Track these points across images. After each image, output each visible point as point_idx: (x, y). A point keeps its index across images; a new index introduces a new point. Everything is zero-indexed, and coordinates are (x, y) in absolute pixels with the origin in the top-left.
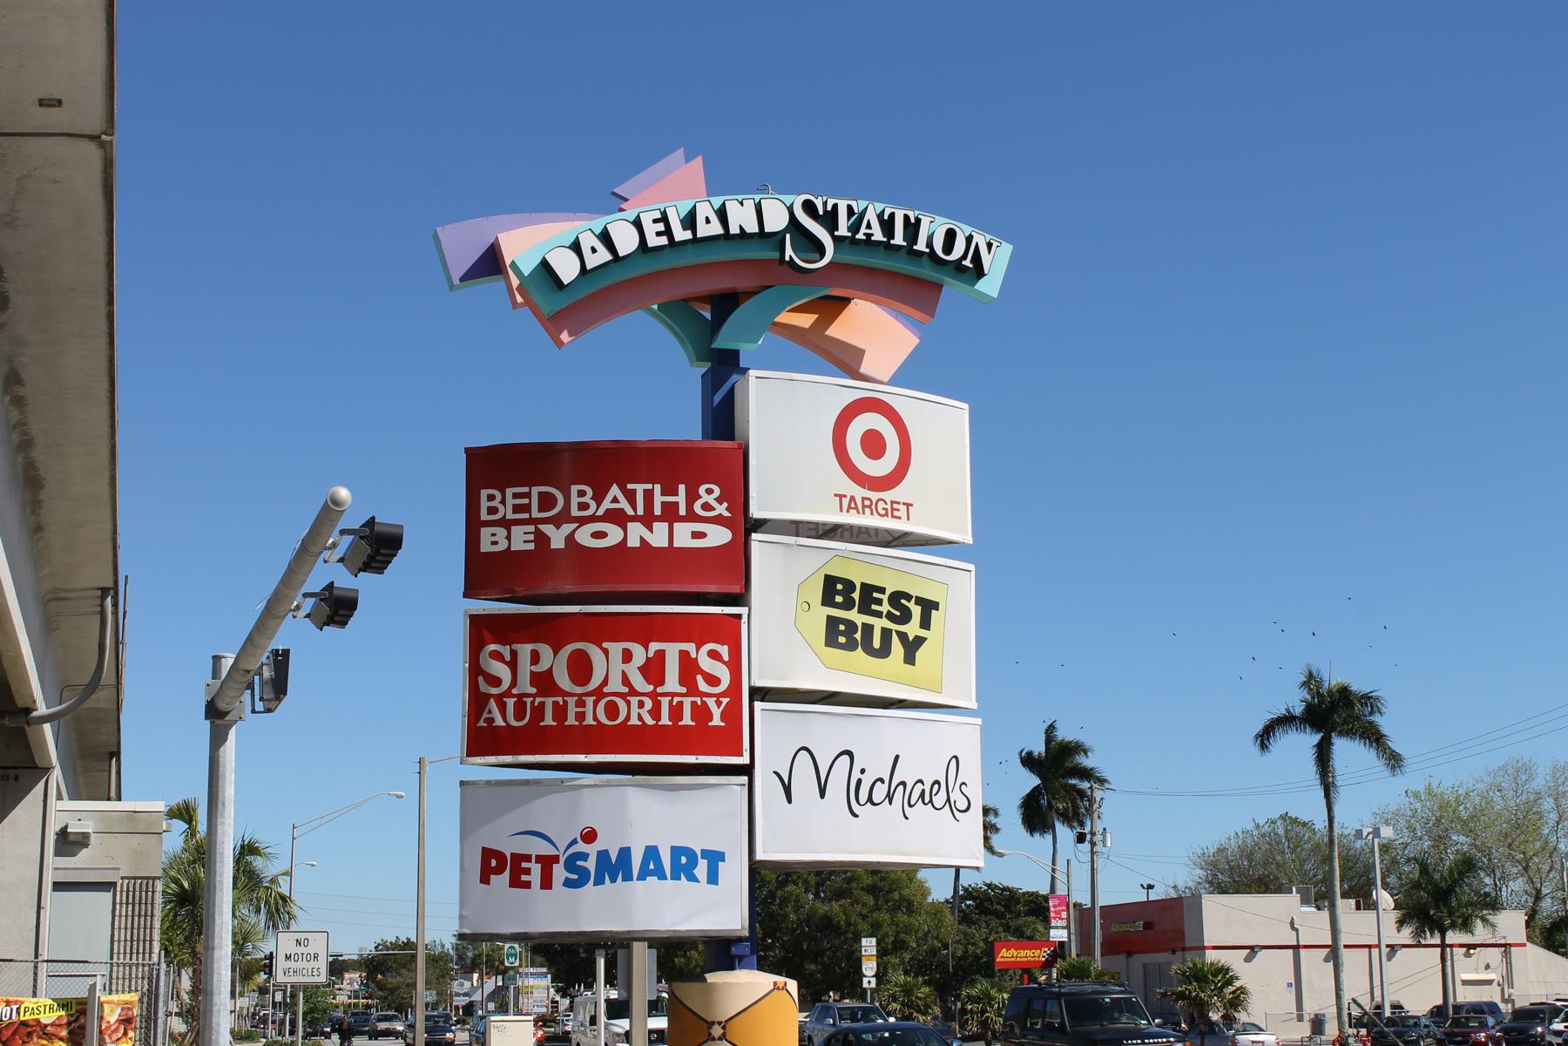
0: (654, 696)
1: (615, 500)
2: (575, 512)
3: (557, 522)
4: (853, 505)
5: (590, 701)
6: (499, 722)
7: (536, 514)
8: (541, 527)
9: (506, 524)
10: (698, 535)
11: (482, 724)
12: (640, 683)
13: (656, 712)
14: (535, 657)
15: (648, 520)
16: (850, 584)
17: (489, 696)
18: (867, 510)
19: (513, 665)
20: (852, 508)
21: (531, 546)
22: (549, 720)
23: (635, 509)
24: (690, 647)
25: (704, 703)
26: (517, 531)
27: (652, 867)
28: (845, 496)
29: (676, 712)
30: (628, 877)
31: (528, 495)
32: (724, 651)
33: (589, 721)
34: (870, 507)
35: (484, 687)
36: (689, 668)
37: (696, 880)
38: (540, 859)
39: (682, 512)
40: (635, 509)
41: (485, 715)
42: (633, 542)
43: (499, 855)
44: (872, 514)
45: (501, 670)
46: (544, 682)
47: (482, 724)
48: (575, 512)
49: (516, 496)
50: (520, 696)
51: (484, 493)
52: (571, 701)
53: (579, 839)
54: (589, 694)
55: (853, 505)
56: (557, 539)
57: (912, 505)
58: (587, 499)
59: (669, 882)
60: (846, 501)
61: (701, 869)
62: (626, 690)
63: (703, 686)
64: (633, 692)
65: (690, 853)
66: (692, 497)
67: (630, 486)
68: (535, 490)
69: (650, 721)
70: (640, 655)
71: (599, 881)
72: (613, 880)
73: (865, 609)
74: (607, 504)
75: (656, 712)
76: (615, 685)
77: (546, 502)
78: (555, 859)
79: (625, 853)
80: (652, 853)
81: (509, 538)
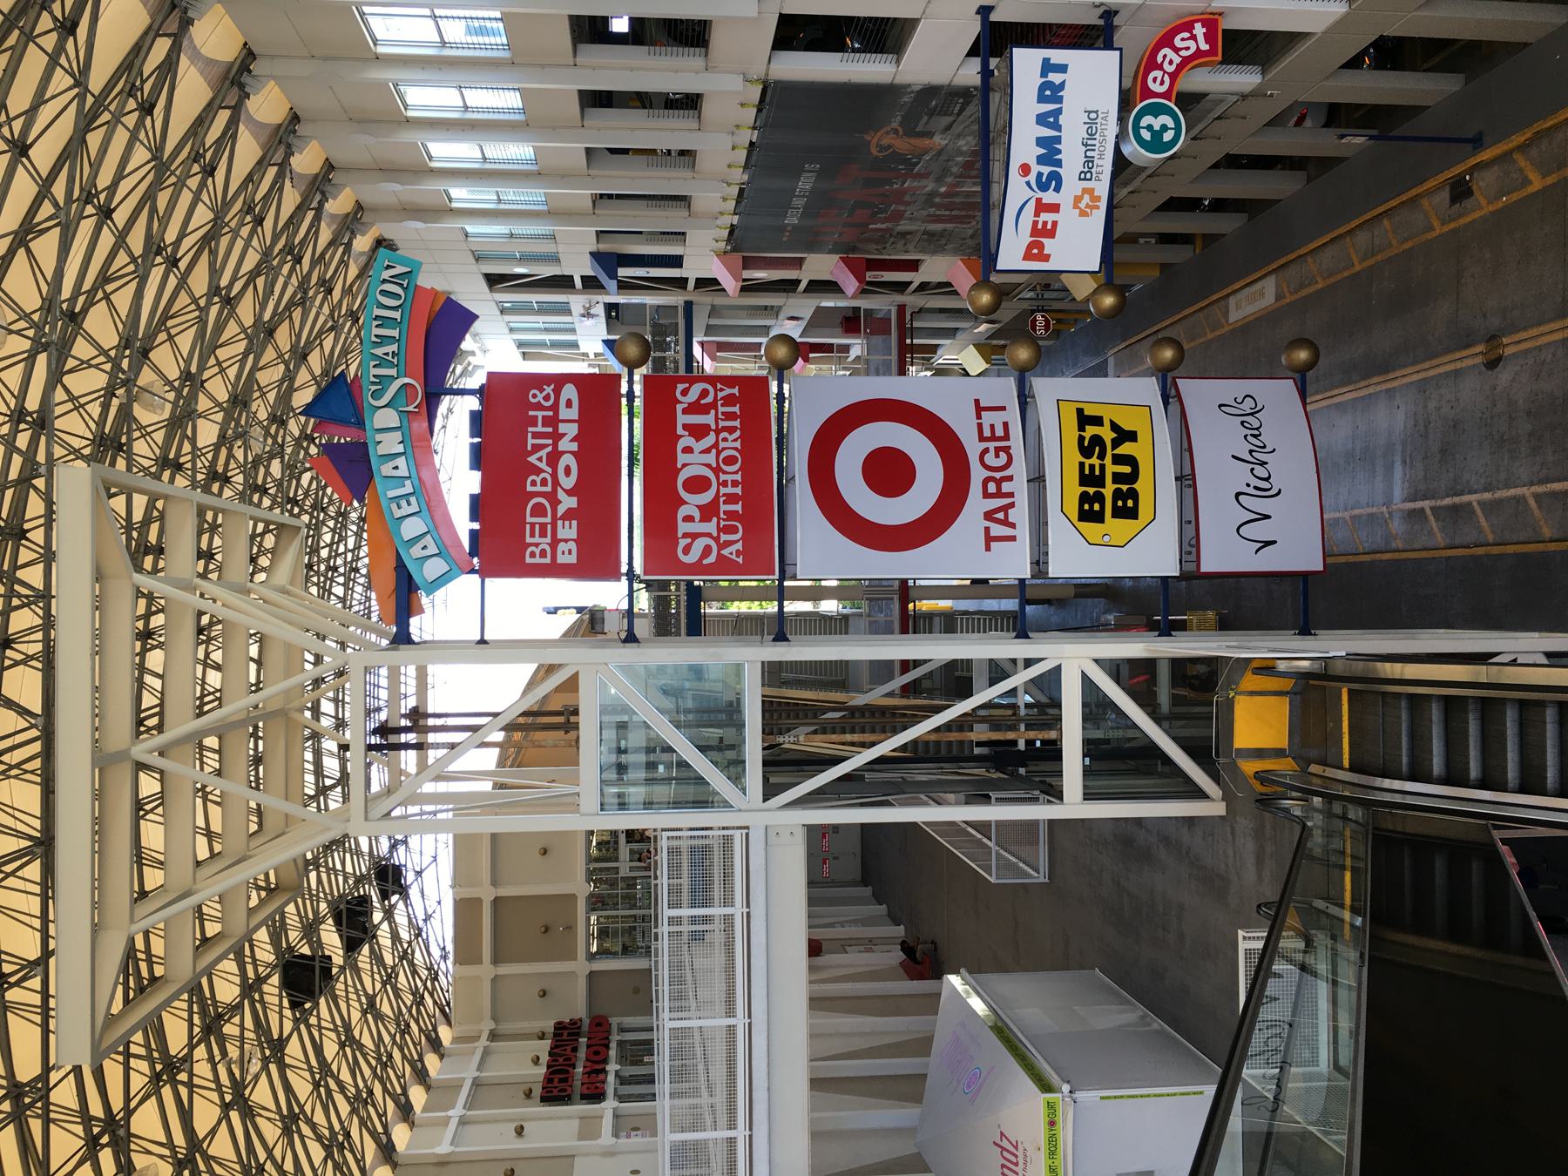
0: (718, 432)
1: (540, 459)
2: (549, 489)
3: (555, 502)
4: (1001, 516)
5: (723, 477)
6: (739, 546)
7: (548, 519)
8: (559, 515)
9: (555, 543)
10: (569, 404)
11: (740, 560)
12: (710, 440)
13: (731, 430)
14: (688, 519)
15: (557, 437)
16: (1084, 498)
18: (1006, 487)
19: (694, 536)
20: (1006, 516)
21: (574, 523)
22: (738, 507)
23: (547, 446)
24: (679, 408)
25: (721, 399)
27: (1052, 120)
28: (987, 530)
29: (729, 416)
30: (1058, 140)
32: (680, 387)
33: (738, 477)
35: (712, 559)
36: (693, 408)
37: (1063, 83)
38: (1037, 214)
39: (551, 413)
40: (547, 446)
41: (734, 557)
42: (574, 447)
43: (1030, 246)
44: (1010, 478)
45: (699, 545)
46: (708, 512)
47: (740, 560)
49: (532, 535)
50: (719, 530)
51: (528, 560)
52: (723, 490)
53: (1026, 179)
54: (718, 478)
55: (1001, 516)
56: (568, 502)
57: (977, 402)
59: (1065, 105)
60: (997, 530)
61: (1055, 78)
62: (714, 451)
63: (710, 399)
64: (716, 445)
65: (1043, 88)
66: (539, 407)
67: (529, 448)
68: (529, 519)
69: (738, 433)
70: (686, 441)
71: (1059, 163)
72: (1059, 152)
73: (1099, 481)
74: (543, 465)
75: (731, 430)
76: (711, 458)
78: (1039, 200)
79: (1041, 142)
80: (1041, 120)
81: (566, 541)
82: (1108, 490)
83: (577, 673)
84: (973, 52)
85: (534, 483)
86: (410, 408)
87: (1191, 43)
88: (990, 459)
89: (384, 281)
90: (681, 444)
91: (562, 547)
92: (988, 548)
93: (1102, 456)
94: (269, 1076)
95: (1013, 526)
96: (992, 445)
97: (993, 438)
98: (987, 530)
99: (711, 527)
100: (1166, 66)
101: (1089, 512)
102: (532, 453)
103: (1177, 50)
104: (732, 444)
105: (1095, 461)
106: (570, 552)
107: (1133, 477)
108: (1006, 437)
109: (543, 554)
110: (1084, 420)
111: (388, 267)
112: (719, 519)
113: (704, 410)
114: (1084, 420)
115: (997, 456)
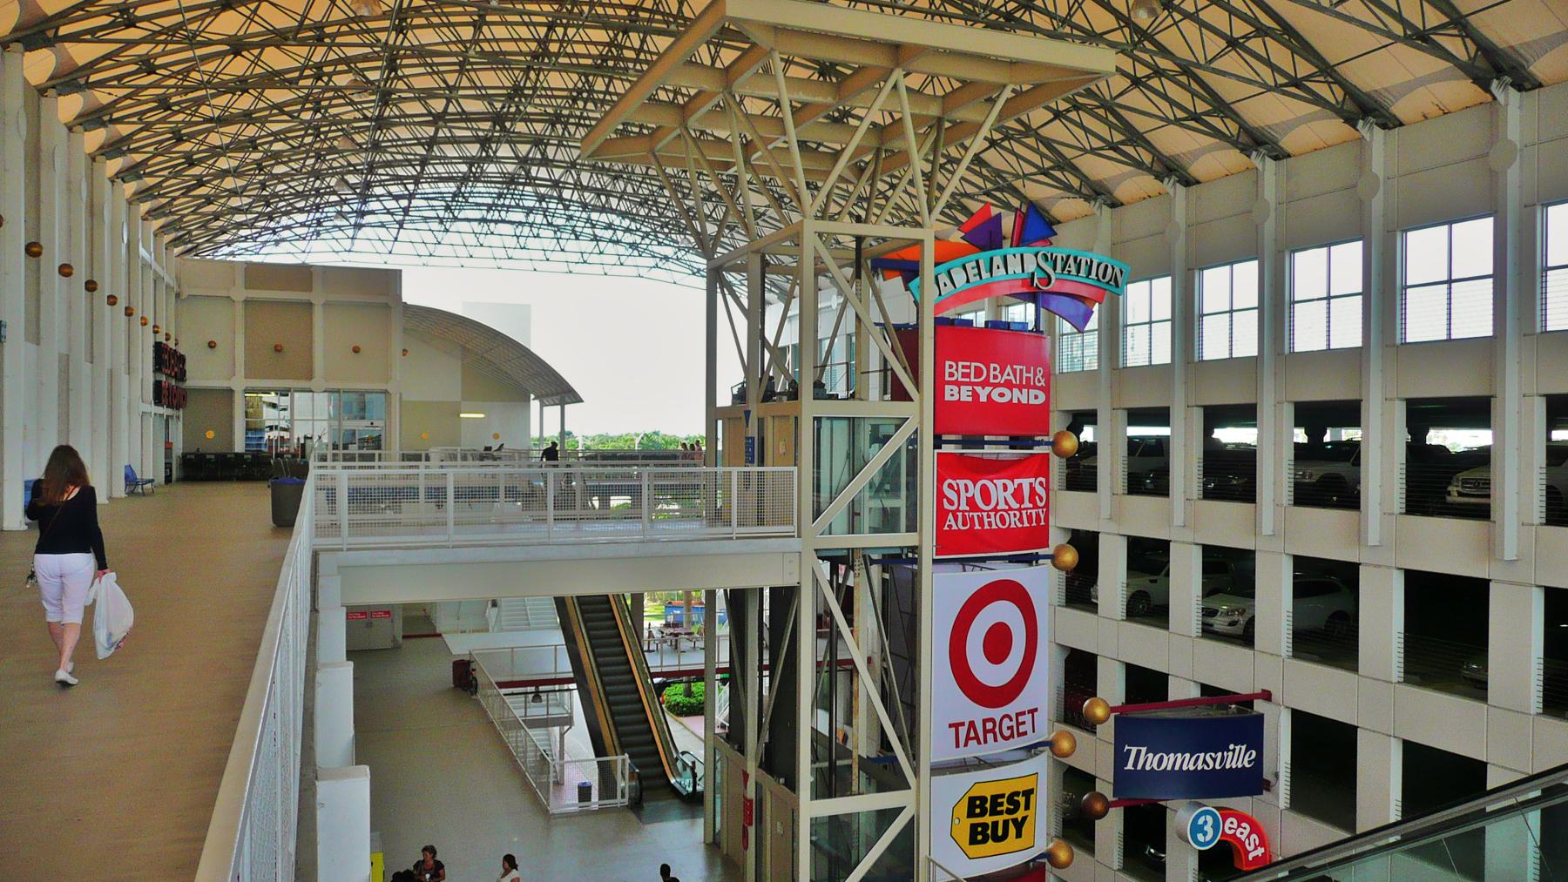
0: (1020, 510)
2: (992, 381)
4: (972, 734)
5: (992, 514)
7: (973, 380)
11: (946, 528)
12: (1015, 505)
13: (1021, 520)
15: (1020, 387)
16: (983, 799)
17: (948, 511)
18: (990, 736)
20: (972, 739)
21: (970, 399)
24: (1032, 480)
26: (963, 388)
28: (963, 724)
31: (969, 367)
33: (994, 527)
34: (992, 731)
35: (947, 506)
36: (1032, 489)
41: (948, 523)
44: (996, 740)
45: (954, 496)
46: (971, 502)
47: (946, 528)
48: (992, 381)
49: (963, 367)
50: (963, 511)
51: (948, 363)
54: (991, 511)
55: (972, 734)
56: (983, 394)
57: (1036, 710)
58: (997, 373)
60: (963, 731)
62: (1007, 508)
64: (1011, 509)
68: (973, 364)
69: (1020, 525)
73: (994, 812)
74: (1005, 377)
75: (1021, 520)
76: (1002, 506)
77: (978, 373)
82: (988, 819)
83: (912, 400)
84: (1205, 689)
85: (995, 369)
86: (1036, 281)
87: (1252, 847)
88: (1006, 722)
89: (1113, 269)
90: (1008, 482)
91: (956, 388)
92: (951, 726)
93: (1009, 812)
94: (454, 127)
95: (966, 745)
96: (1014, 723)
97: (1018, 724)
98: (963, 724)
99: (964, 507)
100: (1240, 830)
101: (976, 805)
102: (1012, 368)
103: (1248, 837)
104: (1013, 521)
105: (1006, 806)
106: (952, 395)
107: (997, 839)
108: (1020, 735)
109: (951, 375)
110: (1028, 793)
111: (1121, 272)
112: (969, 511)
113: (1032, 500)
114: (1028, 793)
115: (1008, 728)
